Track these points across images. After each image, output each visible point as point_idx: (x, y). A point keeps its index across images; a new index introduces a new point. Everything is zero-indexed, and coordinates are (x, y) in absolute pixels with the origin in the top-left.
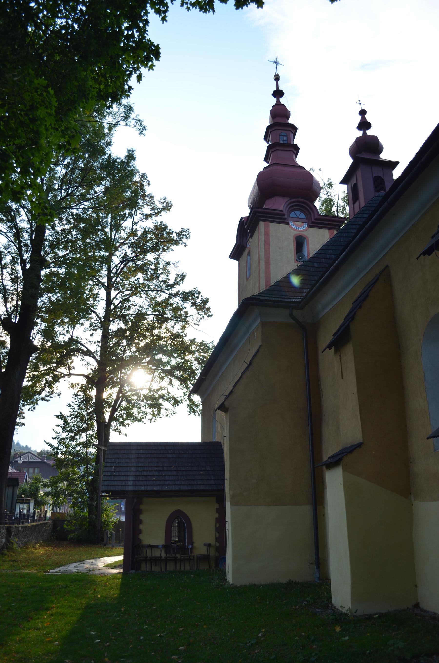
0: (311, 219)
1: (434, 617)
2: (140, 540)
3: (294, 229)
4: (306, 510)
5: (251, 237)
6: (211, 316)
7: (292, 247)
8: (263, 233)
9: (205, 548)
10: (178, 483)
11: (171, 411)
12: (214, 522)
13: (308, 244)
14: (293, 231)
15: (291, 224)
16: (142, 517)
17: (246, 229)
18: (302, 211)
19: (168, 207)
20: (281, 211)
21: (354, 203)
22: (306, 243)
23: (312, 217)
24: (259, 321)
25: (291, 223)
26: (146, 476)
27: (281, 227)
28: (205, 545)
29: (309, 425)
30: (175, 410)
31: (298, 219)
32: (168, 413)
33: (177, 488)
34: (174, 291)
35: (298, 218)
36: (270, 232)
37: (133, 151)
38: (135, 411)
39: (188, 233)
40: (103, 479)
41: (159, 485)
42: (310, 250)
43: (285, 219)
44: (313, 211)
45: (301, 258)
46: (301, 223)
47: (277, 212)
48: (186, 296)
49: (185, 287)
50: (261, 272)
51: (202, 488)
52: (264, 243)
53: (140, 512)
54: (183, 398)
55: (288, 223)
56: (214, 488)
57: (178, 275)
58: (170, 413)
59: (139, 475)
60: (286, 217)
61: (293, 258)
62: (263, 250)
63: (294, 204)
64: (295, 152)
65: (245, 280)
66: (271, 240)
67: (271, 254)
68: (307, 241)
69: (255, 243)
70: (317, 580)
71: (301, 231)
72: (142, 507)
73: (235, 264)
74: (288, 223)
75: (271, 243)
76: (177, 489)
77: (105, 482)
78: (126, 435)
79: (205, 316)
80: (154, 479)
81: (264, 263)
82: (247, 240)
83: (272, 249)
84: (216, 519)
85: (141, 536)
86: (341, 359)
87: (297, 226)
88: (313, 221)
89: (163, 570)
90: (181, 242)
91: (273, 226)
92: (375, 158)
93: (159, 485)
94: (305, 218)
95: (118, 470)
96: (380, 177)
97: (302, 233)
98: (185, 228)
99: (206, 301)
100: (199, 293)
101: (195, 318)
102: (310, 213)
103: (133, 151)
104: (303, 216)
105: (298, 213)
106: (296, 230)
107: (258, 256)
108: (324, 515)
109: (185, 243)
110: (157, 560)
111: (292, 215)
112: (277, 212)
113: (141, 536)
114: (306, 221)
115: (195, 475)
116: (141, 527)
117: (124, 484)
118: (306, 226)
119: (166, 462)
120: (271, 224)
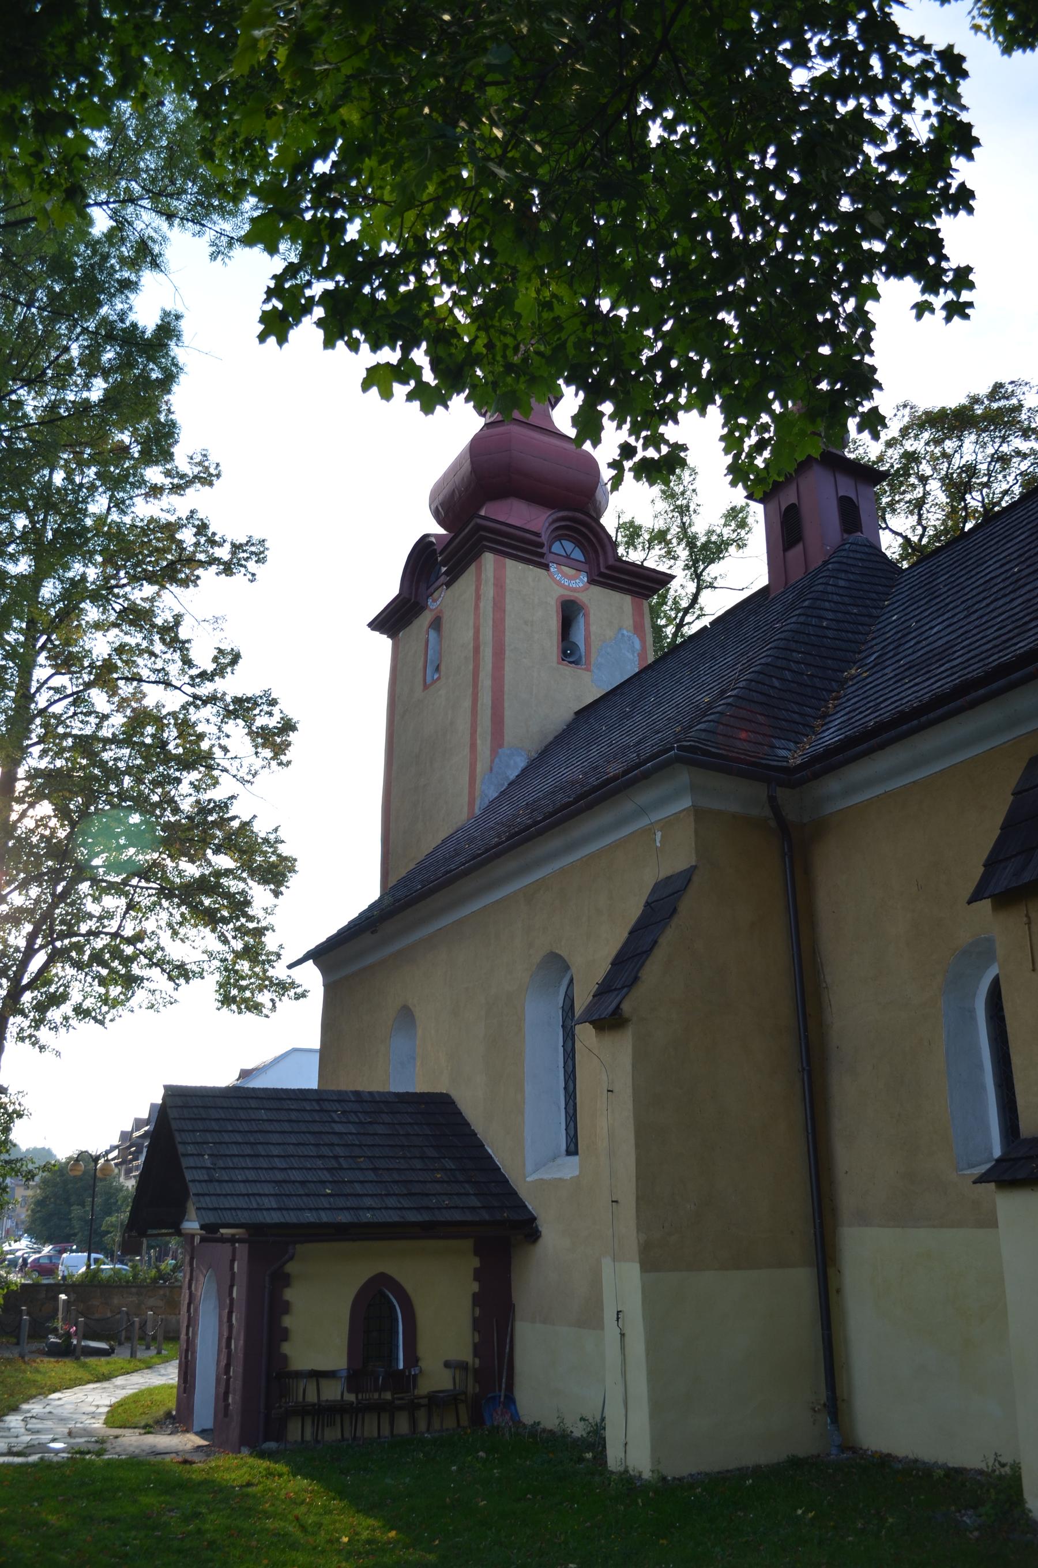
0: (598, 565)
1: (1035, 1522)
2: (285, 1358)
3: (558, 583)
4: (801, 1279)
5: (448, 584)
6: (289, 763)
7: (554, 623)
8: (492, 580)
9: (447, 1374)
10: (391, 1202)
11: (164, 995)
12: (467, 1302)
13: (587, 624)
14: (556, 587)
15: (552, 569)
16: (289, 1294)
17: (425, 566)
18: (578, 544)
19: (206, 478)
20: (538, 535)
21: (786, 549)
22: (581, 620)
23: (601, 561)
24: (686, 803)
25: (553, 568)
26: (303, 1183)
27: (532, 572)
28: (447, 1365)
29: (803, 1069)
30: (176, 995)
31: (567, 560)
32: (154, 1002)
33: (394, 1217)
34: (206, 689)
35: (568, 557)
36: (508, 581)
37: (178, 317)
38: (76, 990)
39: (262, 549)
40: (195, 1191)
41: (347, 1209)
42: (593, 637)
43: (542, 555)
44: (603, 546)
45: (570, 655)
46: (574, 572)
47: (528, 535)
48: (241, 708)
49: (232, 686)
50: (482, 675)
51: (457, 1216)
52: (492, 604)
53: (283, 1280)
54: (205, 966)
55: (546, 567)
56: (486, 1216)
57: (221, 651)
58: (160, 1001)
59: (285, 1181)
60: (544, 550)
61: (555, 649)
62: (491, 623)
63: (568, 523)
64: (553, 401)
65: (420, 687)
66: (507, 601)
67: (507, 633)
68: (586, 616)
69: (454, 601)
70: (834, 1451)
71: (574, 590)
72: (291, 1268)
73: (384, 643)
74: (546, 567)
75: (508, 607)
76: (397, 1219)
77: (202, 1199)
78: (58, 1054)
79: (274, 763)
80: (328, 1191)
81: (490, 654)
82: (431, 589)
83: (509, 622)
84: (475, 1295)
85: (286, 1348)
86: (1029, 923)
87: (565, 575)
88: (603, 570)
89: (347, 1435)
90: (243, 570)
91: (514, 569)
92: (839, 453)
93: (347, 1209)
94: (583, 559)
95: (221, 1163)
96: (850, 499)
97: (576, 594)
98: (257, 537)
99: (288, 726)
100: (273, 703)
101: (245, 764)
102: (596, 551)
103: (178, 317)
104: (577, 554)
105: (569, 546)
106: (563, 586)
107: (471, 633)
108: (838, 1291)
109: (253, 575)
110: (324, 1413)
111: (556, 547)
112: (528, 535)
113: (286, 1348)
114: (586, 567)
115: (425, 1182)
116: (287, 1321)
117: (255, 1206)
118: (585, 579)
119: (338, 1145)
120: (509, 563)
